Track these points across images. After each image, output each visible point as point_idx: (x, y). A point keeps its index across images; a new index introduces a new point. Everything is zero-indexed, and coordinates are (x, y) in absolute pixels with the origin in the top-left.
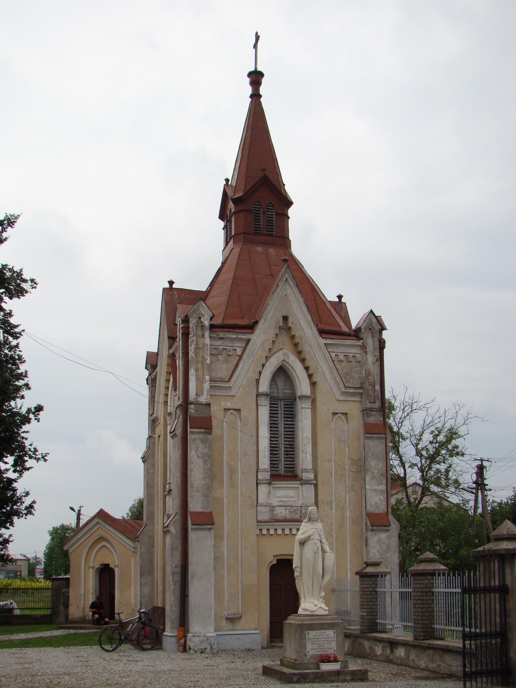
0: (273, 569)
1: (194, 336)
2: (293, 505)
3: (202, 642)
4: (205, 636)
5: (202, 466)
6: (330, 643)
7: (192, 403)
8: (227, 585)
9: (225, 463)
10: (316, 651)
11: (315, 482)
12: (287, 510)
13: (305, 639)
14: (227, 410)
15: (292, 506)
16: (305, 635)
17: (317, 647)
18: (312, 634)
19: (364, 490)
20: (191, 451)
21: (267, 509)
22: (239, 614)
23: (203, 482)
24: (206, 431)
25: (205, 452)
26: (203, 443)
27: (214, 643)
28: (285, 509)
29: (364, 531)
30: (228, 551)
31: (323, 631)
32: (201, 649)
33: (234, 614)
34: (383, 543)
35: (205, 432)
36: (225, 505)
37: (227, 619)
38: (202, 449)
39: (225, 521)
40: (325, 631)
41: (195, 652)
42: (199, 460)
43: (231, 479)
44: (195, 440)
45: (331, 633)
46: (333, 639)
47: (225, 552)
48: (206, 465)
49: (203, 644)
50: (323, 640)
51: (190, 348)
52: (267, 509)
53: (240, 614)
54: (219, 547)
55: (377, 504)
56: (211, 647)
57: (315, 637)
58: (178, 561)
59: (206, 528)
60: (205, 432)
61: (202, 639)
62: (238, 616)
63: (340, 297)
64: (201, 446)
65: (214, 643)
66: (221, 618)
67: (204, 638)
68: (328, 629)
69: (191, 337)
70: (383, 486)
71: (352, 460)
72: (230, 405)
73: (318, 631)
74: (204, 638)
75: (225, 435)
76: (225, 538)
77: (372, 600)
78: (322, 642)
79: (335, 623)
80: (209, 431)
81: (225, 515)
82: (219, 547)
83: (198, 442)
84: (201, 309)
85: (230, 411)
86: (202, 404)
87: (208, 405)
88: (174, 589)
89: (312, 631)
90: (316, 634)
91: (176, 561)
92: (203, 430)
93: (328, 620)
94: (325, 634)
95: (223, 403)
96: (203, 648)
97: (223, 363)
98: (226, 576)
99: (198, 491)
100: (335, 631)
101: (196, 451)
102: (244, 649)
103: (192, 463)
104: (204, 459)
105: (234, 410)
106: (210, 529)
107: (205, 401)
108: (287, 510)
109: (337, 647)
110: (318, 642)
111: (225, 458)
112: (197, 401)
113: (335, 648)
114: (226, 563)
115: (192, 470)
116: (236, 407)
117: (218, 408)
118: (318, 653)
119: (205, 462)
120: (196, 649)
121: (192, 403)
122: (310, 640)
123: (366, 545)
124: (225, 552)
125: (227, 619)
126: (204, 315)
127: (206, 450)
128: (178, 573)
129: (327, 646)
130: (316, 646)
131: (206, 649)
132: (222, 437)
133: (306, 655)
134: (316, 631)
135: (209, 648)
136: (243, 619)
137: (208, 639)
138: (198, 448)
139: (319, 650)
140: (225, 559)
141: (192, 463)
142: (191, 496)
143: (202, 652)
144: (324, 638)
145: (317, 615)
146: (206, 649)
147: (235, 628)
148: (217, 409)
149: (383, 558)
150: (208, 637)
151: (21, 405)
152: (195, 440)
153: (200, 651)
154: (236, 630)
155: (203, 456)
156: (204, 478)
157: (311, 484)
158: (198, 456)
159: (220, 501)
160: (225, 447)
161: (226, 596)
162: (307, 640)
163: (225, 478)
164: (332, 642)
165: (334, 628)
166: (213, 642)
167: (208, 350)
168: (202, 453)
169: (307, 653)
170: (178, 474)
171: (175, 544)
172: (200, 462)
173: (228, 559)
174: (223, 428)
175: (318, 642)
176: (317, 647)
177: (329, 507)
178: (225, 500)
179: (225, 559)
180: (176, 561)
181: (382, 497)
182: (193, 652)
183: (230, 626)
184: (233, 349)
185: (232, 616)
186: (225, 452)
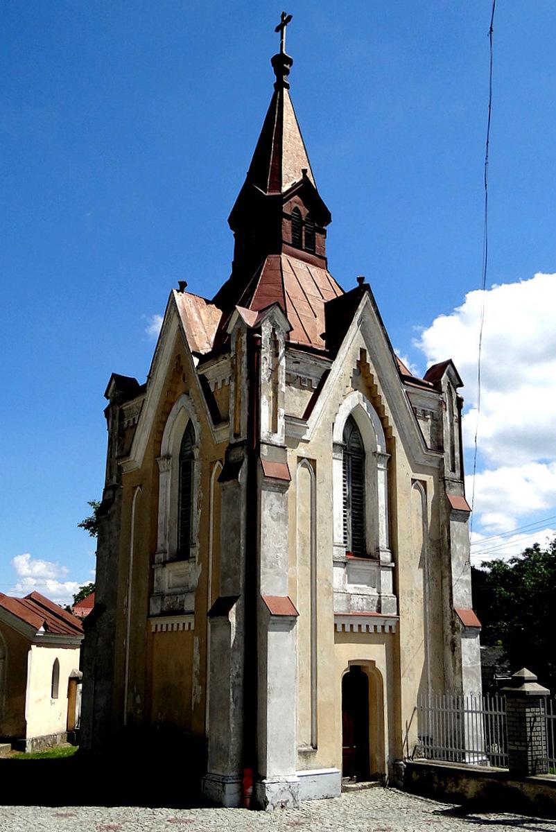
0: (346, 679)
1: (267, 352)
2: (370, 594)
3: (282, 791)
7: (263, 443)
11: (393, 565)
12: (365, 600)
15: (369, 595)
19: (446, 581)
20: (264, 510)
21: (345, 597)
26: (279, 501)
28: (362, 599)
29: (448, 631)
34: (474, 649)
42: (273, 522)
49: (284, 794)
51: (262, 368)
52: (345, 597)
55: (463, 598)
58: (240, 667)
63: (360, 280)
69: (264, 353)
70: (467, 576)
71: (431, 540)
72: (304, 452)
77: (515, 724)
84: (275, 318)
91: (238, 667)
96: (284, 800)
97: (296, 395)
101: (270, 510)
108: (365, 600)
116: (312, 457)
123: (453, 651)
126: (279, 327)
128: (239, 685)
131: (288, 801)
135: (291, 799)
137: (290, 787)
142: (264, 573)
146: (288, 801)
147: (309, 765)
149: (474, 667)
151: (456, 309)
157: (389, 567)
158: (272, 517)
167: (283, 374)
170: (266, 540)
177: (409, 599)
180: (238, 667)
181: (467, 590)
184: (308, 379)
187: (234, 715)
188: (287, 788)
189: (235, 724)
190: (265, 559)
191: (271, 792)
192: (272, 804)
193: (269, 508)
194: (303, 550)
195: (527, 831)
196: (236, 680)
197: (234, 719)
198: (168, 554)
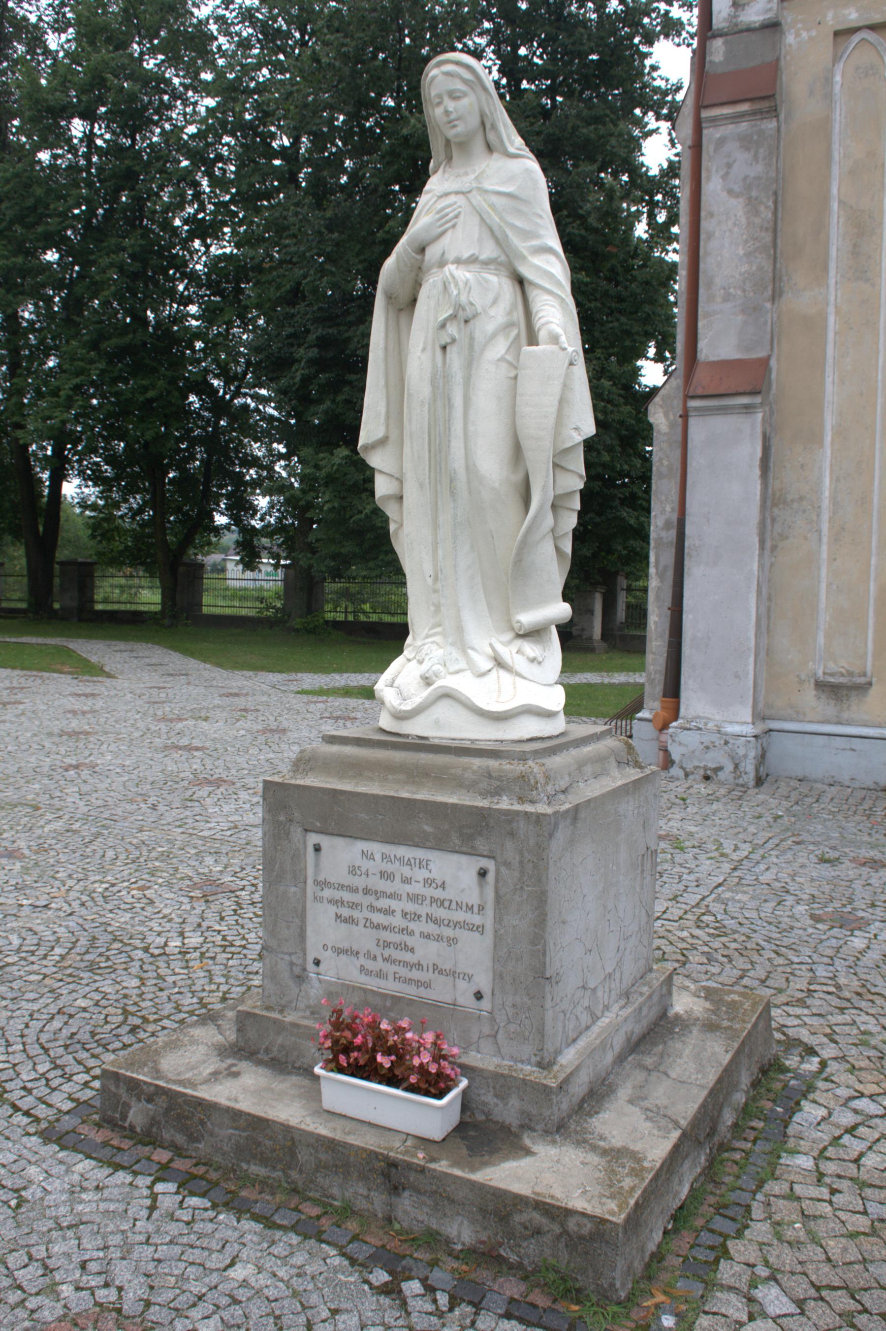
3: (707, 748)
4: (719, 732)
5: (744, 221)
6: (452, 941)
8: (829, 585)
9: (835, 206)
10: (362, 969)
13: (300, 878)
14: (842, 34)
16: (298, 857)
17: (371, 946)
18: (341, 858)
20: (709, 179)
22: (865, 675)
23: (745, 268)
24: (757, 106)
25: (752, 175)
26: (748, 149)
27: (745, 756)
30: (835, 480)
31: (403, 851)
32: (706, 768)
33: (851, 674)
35: (754, 113)
36: (831, 335)
37: (820, 685)
38: (746, 165)
39: (829, 387)
40: (420, 854)
41: (687, 775)
42: (733, 202)
43: (855, 251)
44: (722, 141)
45: (456, 874)
46: (476, 919)
47: (827, 481)
48: (757, 213)
50: (410, 907)
53: (869, 673)
54: (802, 467)
56: (736, 766)
57: (359, 882)
58: (673, 510)
59: (734, 407)
60: (754, 113)
61: (707, 739)
62: (862, 680)
64: (742, 157)
65: (745, 756)
66: (801, 682)
67: (715, 737)
68: (440, 844)
73: (376, 848)
74: (715, 737)
75: (838, 117)
76: (828, 439)
78: (397, 921)
79: (482, 814)
80: (765, 105)
81: (829, 370)
82: (802, 467)
83: (732, 146)
85: (856, 38)
86: (749, 30)
87: (773, 26)
88: (659, 588)
89: (340, 842)
90: (366, 865)
92: (744, 107)
93: (459, 783)
94: (421, 874)
95: (830, 15)
96: (713, 766)
98: (824, 555)
99: (727, 298)
100: (490, 865)
101: (724, 177)
102: (869, 783)
103: (711, 215)
104: (750, 199)
105: (873, 28)
106: (748, 409)
107: (761, 18)
109: (498, 977)
110: (378, 918)
111: (834, 191)
112: (736, 25)
113: (484, 981)
114: (825, 516)
115: (710, 236)
117: (814, 33)
118: (372, 983)
119: (752, 205)
120: (689, 767)
121: (720, 34)
122: (327, 893)
124: (827, 481)
125: (820, 685)
127: (759, 168)
129: (428, 952)
130: (364, 939)
131: (720, 769)
132: (825, 126)
133: (301, 978)
134: (362, 845)
135: (729, 767)
136: (873, 691)
137: (726, 743)
138: (729, 166)
139: (380, 964)
140: (826, 503)
141: (711, 215)
143: (707, 778)
144: (414, 898)
145: (422, 745)
146: (720, 769)
147: (845, 715)
148: (811, 38)
150: (727, 735)
152: (722, 141)
153: (702, 772)
154: (848, 723)
155: (748, 187)
156: (748, 255)
158: (730, 192)
159: (814, 325)
160: (836, 156)
161: (824, 618)
162: (310, 888)
163: (833, 252)
164: (463, 935)
165: (480, 844)
166: (741, 752)
168: (746, 178)
169: (311, 967)
171: (665, 463)
172: (738, 206)
173: (835, 501)
174: (829, 96)
175: (378, 918)
176: (371, 946)
178: (831, 319)
179: (826, 503)
182: (681, 774)
183: (831, 710)
185: (842, 680)
186: (835, 170)
187: (657, 597)
188: (719, 742)
189: (659, 616)
190: (709, 285)
191: (680, 744)
192: (682, 767)
193: (721, 173)
194: (855, 246)
195: (256, 1261)
196: (663, 534)
197: (659, 607)
198: (563, 339)
